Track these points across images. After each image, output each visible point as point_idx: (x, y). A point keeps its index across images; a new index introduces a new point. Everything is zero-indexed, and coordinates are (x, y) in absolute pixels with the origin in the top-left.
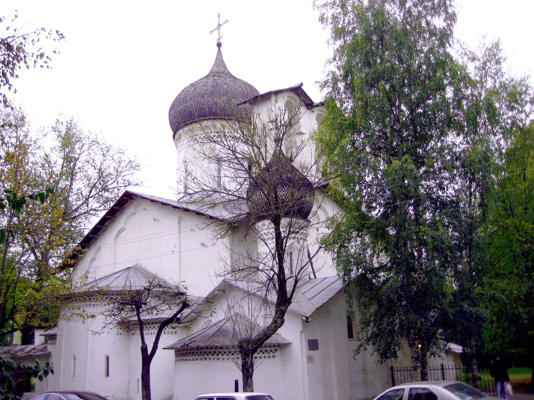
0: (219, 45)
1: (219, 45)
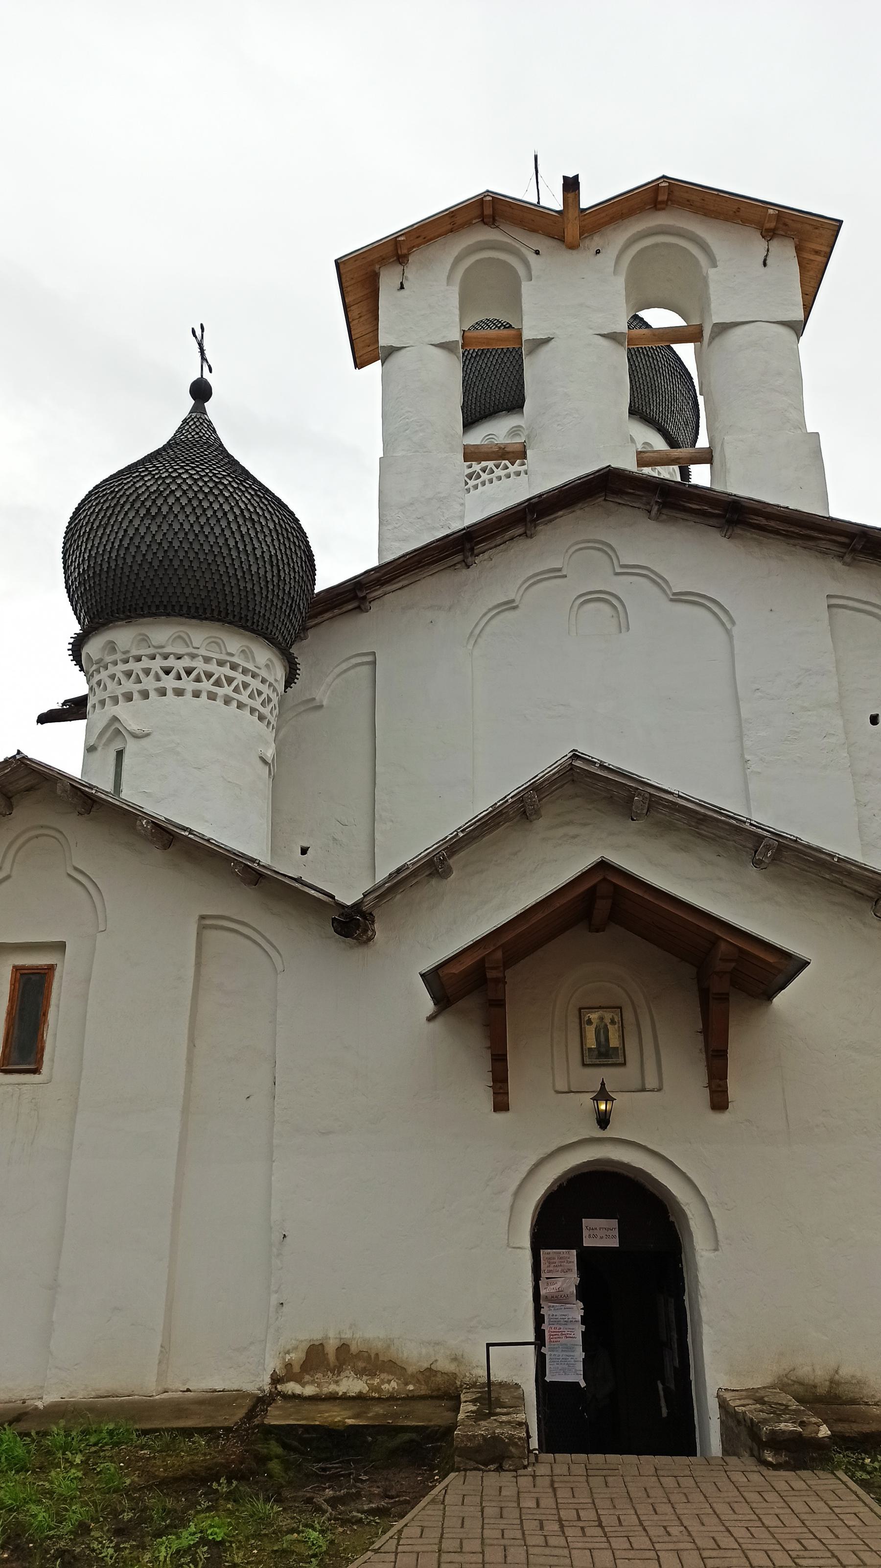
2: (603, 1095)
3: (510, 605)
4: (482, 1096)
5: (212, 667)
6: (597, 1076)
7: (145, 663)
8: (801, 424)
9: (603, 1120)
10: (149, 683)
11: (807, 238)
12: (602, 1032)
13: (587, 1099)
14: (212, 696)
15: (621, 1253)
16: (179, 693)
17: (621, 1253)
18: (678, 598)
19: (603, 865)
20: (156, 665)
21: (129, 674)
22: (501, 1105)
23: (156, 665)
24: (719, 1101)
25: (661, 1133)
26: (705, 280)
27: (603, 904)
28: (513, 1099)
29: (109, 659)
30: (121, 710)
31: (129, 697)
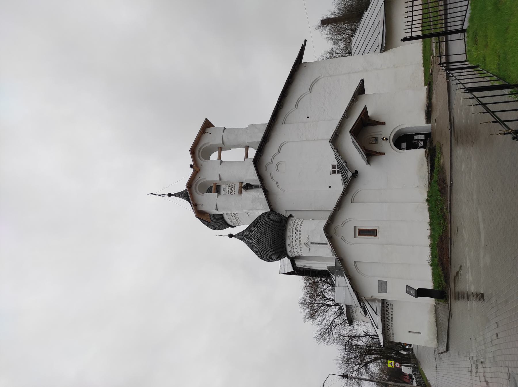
0: (170, 195)
1: (170, 195)
2: (383, 139)
3: (277, 183)
4: (383, 157)
5: (295, 225)
6: (380, 140)
7: (294, 237)
8: (246, 128)
9: (387, 139)
10: (298, 237)
11: (207, 125)
12: (373, 141)
13: (383, 142)
14: (301, 225)
15: (405, 140)
16: (300, 231)
17: (405, 140)
18: (279, 151)
19: (350, 132)
20: (294, 235)
21: (295, 241)
22: (384, 154)
23: (294, 235)
24: (384, 123)
25: (389, 131)
26: (211, 145)
27: (356, 132)
28: (383, 152)
29: (292, 246)
30: (302, 243)
31: (300, 241)
